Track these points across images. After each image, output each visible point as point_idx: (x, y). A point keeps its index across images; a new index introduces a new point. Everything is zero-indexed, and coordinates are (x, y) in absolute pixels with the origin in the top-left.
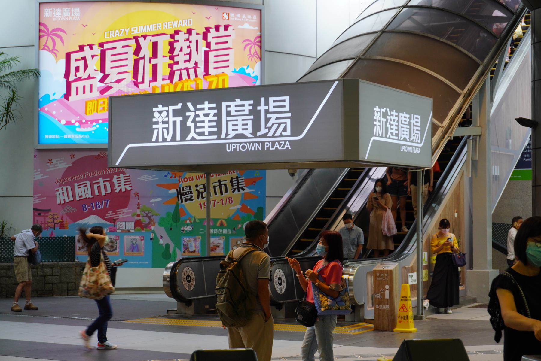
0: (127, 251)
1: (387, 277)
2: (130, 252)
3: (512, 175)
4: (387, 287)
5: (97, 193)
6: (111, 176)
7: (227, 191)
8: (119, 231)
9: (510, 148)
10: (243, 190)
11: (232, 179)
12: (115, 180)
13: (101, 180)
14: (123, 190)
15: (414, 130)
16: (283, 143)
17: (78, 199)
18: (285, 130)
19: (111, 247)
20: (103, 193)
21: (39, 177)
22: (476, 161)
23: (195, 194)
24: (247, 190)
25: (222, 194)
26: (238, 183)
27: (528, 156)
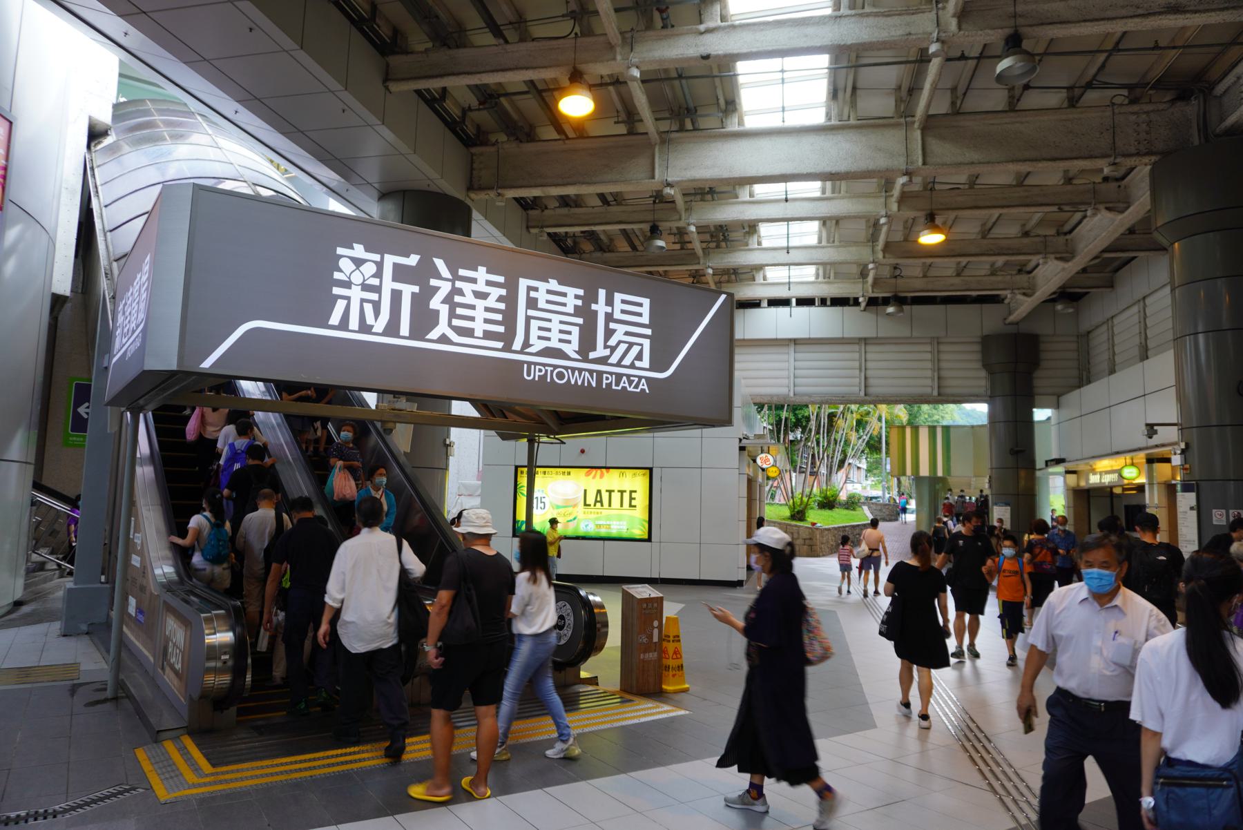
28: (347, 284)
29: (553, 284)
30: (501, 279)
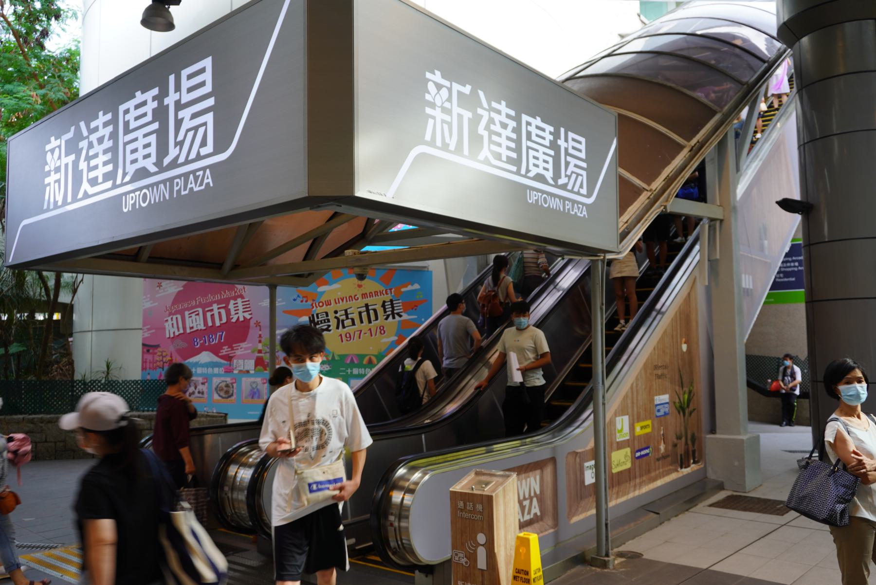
0: (246, 397)
1: (481, 513)
2: (249, 399)
3: (767, 298)
4: (481, 538)
5: (210, 324)
6: (227, 301)
7: (377, 319)
8: (236, 372)
9: (767, 252)
10: (400, 316)
11: (384, 302)
12: (231, 306)
13: (215, 307)
14: (241, 319)
15: (567, 164)
16: (201, 173)
17: (188, 331)
18: (204, 143)
19: (227, 392)
20: (218, 324)
21: (148, 305)
22: (717, 260)
23: (333, 323)
24: (405, 316)
25: (370, 322)
26: (393, 307)
27: (797, 264)
28: (433, 105)
29: (538, 121)
30: (172, 78)
